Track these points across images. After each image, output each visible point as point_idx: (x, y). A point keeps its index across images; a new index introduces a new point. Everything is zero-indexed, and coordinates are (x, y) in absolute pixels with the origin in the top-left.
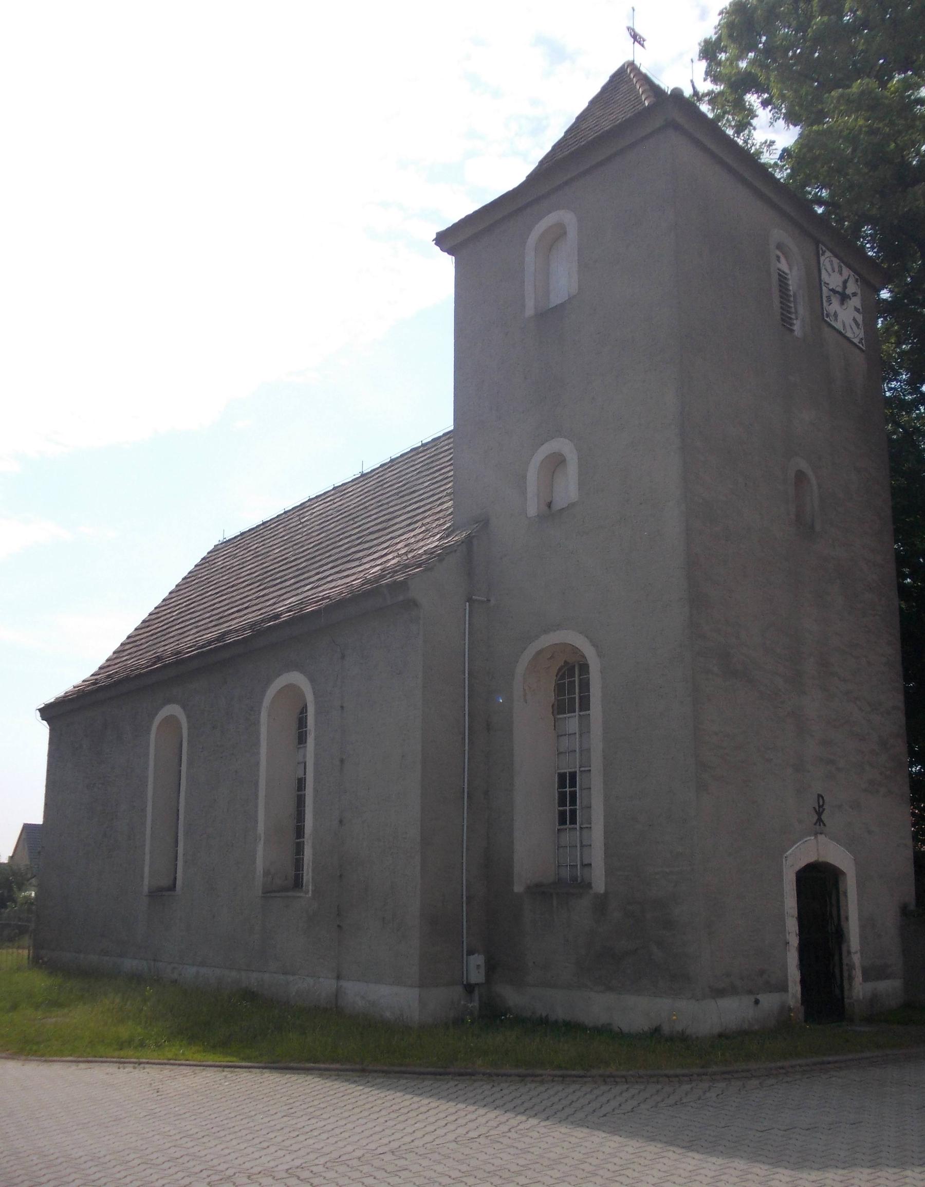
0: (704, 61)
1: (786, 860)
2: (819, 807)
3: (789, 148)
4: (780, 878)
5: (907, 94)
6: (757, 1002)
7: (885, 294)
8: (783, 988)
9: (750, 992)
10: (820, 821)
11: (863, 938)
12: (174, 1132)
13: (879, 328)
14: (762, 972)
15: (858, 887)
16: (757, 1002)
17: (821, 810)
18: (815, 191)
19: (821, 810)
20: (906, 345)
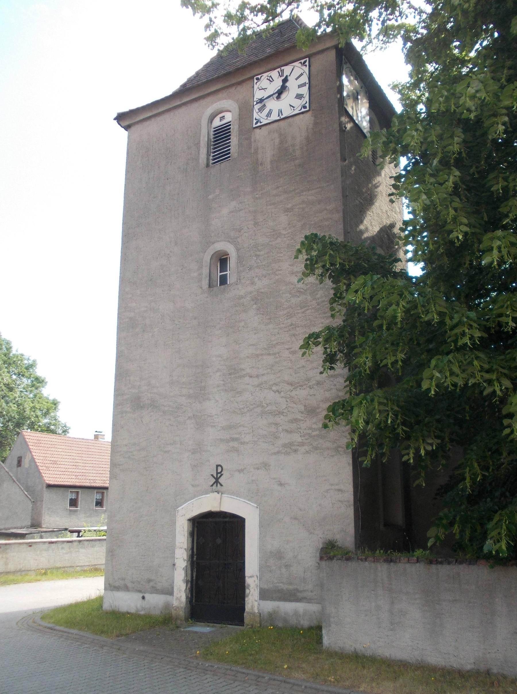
0: (409, 65)
1: (178, 512)
2: (217, 473)
3: (313, 27)
4: (173, 523)
5: (415, 186)
6: (143, 598)
7: (337, 26)
8: (170, 592)
9: (140, 591)
10: (217, 481)
11: (263, 568)
12: (359, 115)
13: (424, 66)
14: (149, 581)
15: (261, 526)
16: (143, 598)
17: (219, 475)
18: (325, 30)
19: (219, 475)
20: (326, 33)
